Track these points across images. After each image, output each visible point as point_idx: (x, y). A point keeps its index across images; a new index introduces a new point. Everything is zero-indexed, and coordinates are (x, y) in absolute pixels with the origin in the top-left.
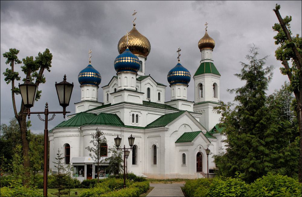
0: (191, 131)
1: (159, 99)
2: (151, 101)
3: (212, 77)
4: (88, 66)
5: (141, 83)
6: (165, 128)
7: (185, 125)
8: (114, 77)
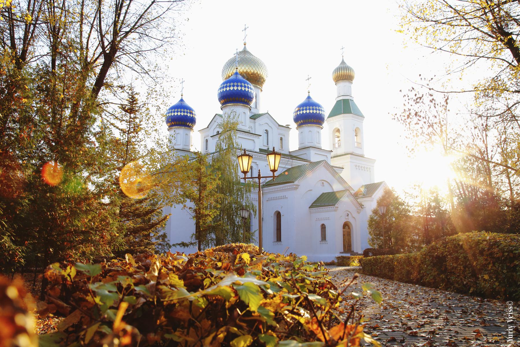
3: (353, 119)
4: (180, 101)
6: (294, 185)
7: (323, 181)
8: (216, 114)
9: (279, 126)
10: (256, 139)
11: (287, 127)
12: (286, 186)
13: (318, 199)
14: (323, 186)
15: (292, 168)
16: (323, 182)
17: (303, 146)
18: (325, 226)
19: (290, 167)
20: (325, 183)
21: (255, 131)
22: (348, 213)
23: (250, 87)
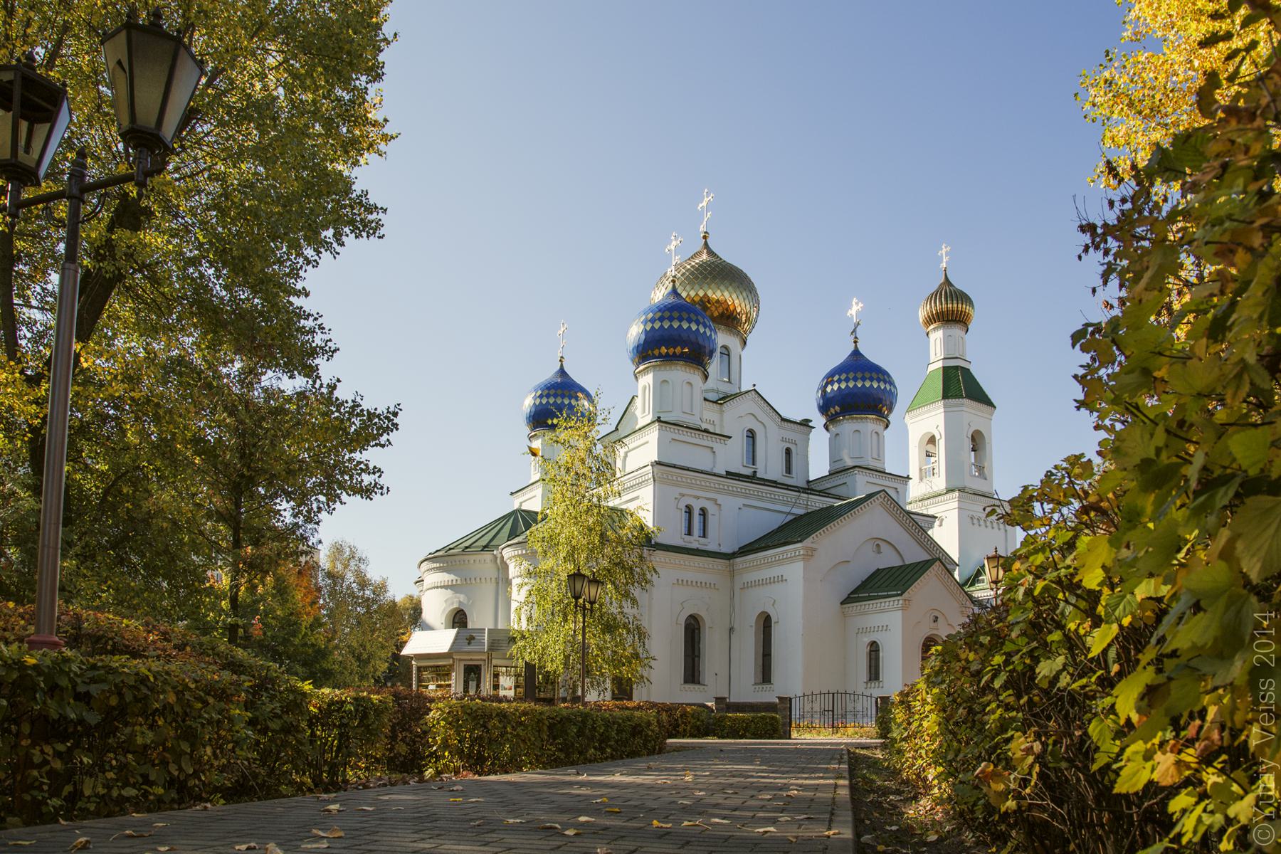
0: (899, 563)
1: (788, 469)
2: (759, 475)
5: (722, 412)
7: (879, 542)
9: (784, 420)
10: (717, 445)
11: (805, 423)
12: (786, 552)
13: (863, 582)
14: (879, 552)
15: (808, 513)
16: (878, 544)
17: (838, 466)
18: (877, 645)
19: (801, 511)
20: (884, 546)
21: (722, 426)
22: (937, 614)
23: (701, 320)
